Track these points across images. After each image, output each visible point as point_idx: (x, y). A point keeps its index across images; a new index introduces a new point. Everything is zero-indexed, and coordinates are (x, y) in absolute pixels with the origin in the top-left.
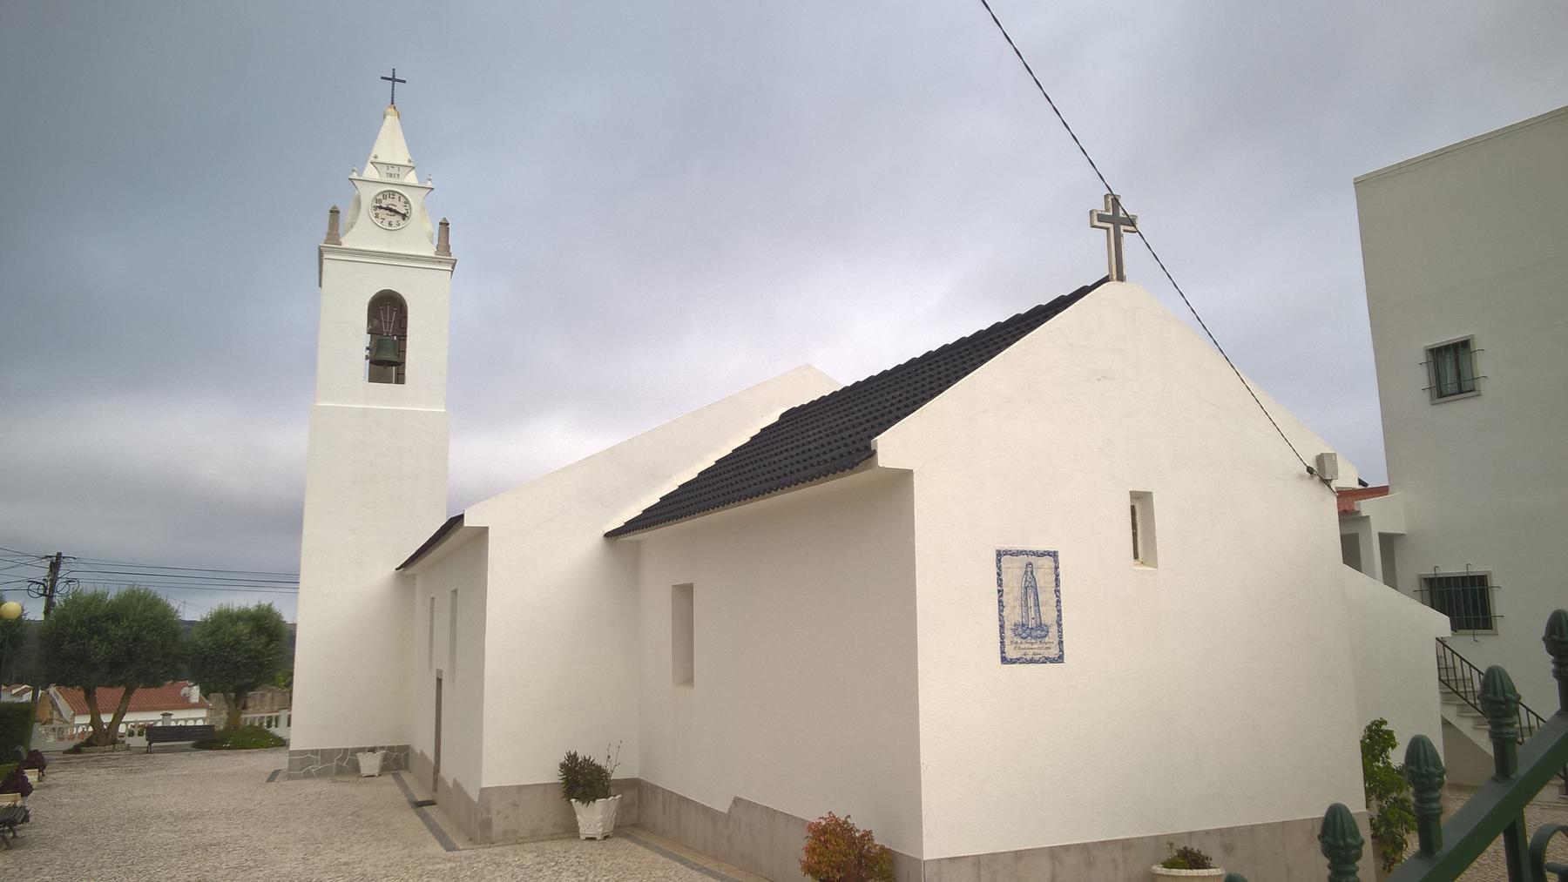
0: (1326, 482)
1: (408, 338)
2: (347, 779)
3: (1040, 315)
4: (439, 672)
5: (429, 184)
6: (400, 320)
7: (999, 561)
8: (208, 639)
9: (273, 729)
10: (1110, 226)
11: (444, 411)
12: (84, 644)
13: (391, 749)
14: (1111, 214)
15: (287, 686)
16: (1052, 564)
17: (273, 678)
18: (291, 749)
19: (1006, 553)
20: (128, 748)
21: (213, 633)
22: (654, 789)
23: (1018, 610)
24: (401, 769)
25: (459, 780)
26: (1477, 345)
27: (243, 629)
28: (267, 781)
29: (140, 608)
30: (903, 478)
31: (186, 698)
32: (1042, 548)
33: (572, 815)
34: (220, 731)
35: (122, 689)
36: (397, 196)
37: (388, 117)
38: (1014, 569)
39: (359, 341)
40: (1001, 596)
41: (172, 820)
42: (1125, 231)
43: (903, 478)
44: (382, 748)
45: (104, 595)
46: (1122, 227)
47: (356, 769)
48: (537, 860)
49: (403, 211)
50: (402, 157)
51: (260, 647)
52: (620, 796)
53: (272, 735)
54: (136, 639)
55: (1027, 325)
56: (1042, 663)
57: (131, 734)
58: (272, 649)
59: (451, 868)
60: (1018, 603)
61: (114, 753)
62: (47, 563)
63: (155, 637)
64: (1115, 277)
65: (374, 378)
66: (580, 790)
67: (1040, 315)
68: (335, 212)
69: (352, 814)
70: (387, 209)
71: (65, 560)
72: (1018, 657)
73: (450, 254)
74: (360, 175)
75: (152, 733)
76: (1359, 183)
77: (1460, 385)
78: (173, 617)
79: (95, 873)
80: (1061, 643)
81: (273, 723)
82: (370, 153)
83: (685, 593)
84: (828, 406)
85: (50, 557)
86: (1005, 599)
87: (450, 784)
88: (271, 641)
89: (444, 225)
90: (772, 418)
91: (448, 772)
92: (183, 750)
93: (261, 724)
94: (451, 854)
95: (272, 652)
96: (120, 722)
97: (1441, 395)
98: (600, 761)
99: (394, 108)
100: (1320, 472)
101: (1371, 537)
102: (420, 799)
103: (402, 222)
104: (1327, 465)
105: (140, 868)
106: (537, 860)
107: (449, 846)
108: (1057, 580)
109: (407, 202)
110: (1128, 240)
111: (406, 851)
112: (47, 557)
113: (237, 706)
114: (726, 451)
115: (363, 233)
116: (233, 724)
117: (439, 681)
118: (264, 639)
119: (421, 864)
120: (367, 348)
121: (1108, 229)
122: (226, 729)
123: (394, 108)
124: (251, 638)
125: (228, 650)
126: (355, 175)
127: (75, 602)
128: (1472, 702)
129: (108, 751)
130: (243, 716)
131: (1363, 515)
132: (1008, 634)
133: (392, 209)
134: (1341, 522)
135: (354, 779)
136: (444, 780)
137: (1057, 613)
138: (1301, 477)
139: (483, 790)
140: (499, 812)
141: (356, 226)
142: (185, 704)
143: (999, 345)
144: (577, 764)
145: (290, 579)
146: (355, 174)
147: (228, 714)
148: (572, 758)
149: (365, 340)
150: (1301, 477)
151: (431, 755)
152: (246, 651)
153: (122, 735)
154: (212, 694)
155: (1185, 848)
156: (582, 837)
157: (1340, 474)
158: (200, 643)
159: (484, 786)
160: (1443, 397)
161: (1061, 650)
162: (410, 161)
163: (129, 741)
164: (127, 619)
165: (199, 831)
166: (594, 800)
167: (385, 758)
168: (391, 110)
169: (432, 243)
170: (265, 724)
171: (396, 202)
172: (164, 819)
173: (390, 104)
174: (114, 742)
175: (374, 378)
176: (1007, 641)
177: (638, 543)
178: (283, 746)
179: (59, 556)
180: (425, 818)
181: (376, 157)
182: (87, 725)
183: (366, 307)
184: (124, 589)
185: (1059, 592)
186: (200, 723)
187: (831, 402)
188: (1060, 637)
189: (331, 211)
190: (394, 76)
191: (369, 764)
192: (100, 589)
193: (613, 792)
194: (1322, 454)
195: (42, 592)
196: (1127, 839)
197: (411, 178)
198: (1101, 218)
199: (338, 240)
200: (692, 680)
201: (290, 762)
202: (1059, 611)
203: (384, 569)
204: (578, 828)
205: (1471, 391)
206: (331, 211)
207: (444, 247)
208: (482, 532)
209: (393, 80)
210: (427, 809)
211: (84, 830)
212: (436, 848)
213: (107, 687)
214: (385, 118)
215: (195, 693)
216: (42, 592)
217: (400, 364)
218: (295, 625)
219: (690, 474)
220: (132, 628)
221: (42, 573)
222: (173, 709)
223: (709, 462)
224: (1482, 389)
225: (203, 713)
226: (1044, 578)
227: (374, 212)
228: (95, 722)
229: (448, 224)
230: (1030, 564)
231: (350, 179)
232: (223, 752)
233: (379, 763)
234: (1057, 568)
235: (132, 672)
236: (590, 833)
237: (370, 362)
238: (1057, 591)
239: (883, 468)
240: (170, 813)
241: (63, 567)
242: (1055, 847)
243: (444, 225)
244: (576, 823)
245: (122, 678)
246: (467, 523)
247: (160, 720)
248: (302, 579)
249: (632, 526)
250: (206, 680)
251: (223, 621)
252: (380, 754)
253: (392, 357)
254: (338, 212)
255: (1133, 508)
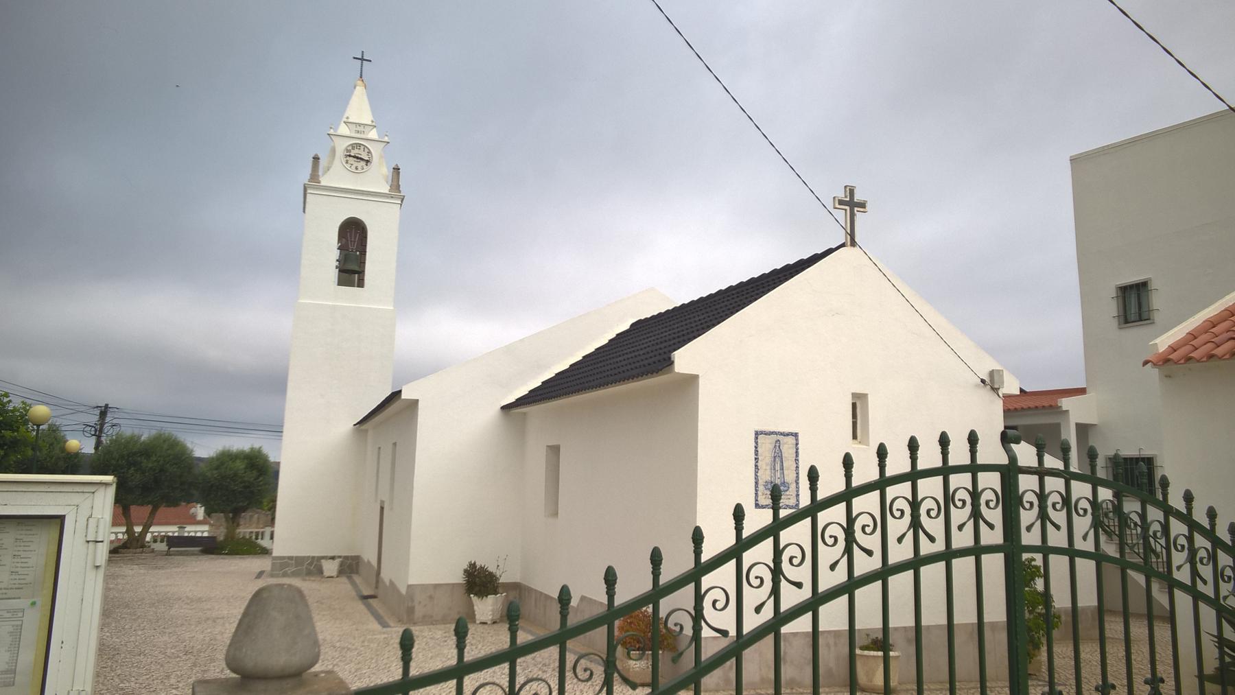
0: (995, 390)
1: (367, 254)
2: (313, 579)
3: (815, 259)
4: (382, 502)
5: (386, 139)
6: (362, 240)
7: (756, 438)
8: (215, 472)
9: (259, 541)
10: (847, 208)
11: (392, 308)
12: (123, 473)
13: (346, 558)
14: (848, 199)
15: (269, 510)
16: (794, 442)
17: (261, 503)
18: (274, 555)
19: (762, 433)
20: (153, 551)
21: (217, 468)
22: (530, 590)
23: (768, 472)
24: (354, 573)
25: (393, 580)
26: (1153, 285)
27: (240, 465)
28: (256, 578)
29: (165, 447)
30: (692, 380)
31: (194, 517)
32: (787, 430)
33: (471, 606)
34: (221, 541)
35: (150, 508)
36: (362, 147)
37: (358, 88)
38: (766, 444)
39: (332, 254)
40: (757, 462)
41: (189, 601)
42: (858, 211)
43: (692, 380)
44: (340, 557)
45: (139, 437)
46: (856, 209)
47: (320, 571)
48: (445, 635)
49: (367, 159)
50: (367, 118)
51: (252, 479)
52: (505, 594)
53: (259, 546)
54: (161, 470)
55: (785, 276)
56: (784, 508)
57: (155, 541)
58: (261, 481)
59: (385, 638)
60: (768, 468)
61: (143, 554)
62: (97, 412)
63: (175, 469)
64: (849, 244)
65: (341, 283)
66: (477, 589)
67: (815, 259)
68: (316, 159)
69: (318, 602)
70: (354, 157)
71: (111, 410)
72: (767, 504)
73: (400, 192)
74: (335, 131)
75: (172, 542)
76: (1073, 160)
77: (1140, 315)
78: (189, 454)
79: (140, 633)
80: (798, 495)
81: (260, 537)
82: (343, 116)
83: (555, 450)
84: (699, 307)
85: (100, 407)
86: (759, 464)
87: (388, 584)
88: (260, 475)
89: (397, 169)
90: (625, 326)
91: (386, 575)
92: (193, 554)
93: (251, 537)
94: (385, 629)
95: (261, 483)
96: (147, 532)
97: (1126, 322)
98: (492, 568)
99: (362, 81)
100: (991, 383)
101: (1069, 426)
102: (366, 593)
103: (365, 167)
104: (996, 378)
105: (170, 631)
106: (445, 635)
107: (384, 625)
108: (797, 452)
109: (369, 152)
110: (859, 217)
111: (354, 626)
112: (98, 407)
113: (233, 523)
114: (590, 349)
115: (337, 175)
116: (230, 536)
117: (382, 508)
118: (255, 473)
119: (364, 635)
120: (337, 261)
121: (846, 210)
122: (225, 540)
123: (362, 81)
124: (245, 472)
125: (228, 480)
126: (332, 132)
127: (116, 442)
128: (1137, 551)
129: (139, 553)
130: (238, 531)
131: (1064, 409)
132: (761, 488)
133: (358, 157)
134: (1005, 417)
135: (319, 579)
136: (383, 582)
137: (795, 475)
138: (977, 386)
139: (409, 586)
140: (420, 602)
141: (331, 170)
142: (193, 521)
143: (781, 279)
144: (475, 571)
145: (277, 430)
146: (332, 130)
147: (227, 528)
148: (473, 565)
149: (335, 254)
150: (977, 386)
151: (374, 563)
152: (241, 483)
153: (148, 542)
154: (213, 514)
155: (877, 638)
156: (478, 622)
157: (1005, 384)
158: (208, 474)
159: (410, 583)
160: (1142, 320)
161: (798, 501)
162: (372, 122)
163: (154, 546)
164: (156, 455)
165: (209, 609)
166: (487, 596)
167: (341, 565)
168: (360, 82)
169: (387, 182)
170: (254, 537)
171: (361, 152)
172: (183, 601)
173: (359, 77)
174: (143, 546)
175: (341, 283)
176: (760, 493)
177: (525, 414)
178: (267, 553)
179: (106, 406)
180: (369, 607)
181: (347, 118)
182: (123, 533)
183: (337, 230)
184: (154, 432)
185: (798, 460)
186: (206, 534)
187: (665, 317)
188: (798, 491)
189: (314, 158)
190: (362, 56)
191: (330, 568)
192: (136, 432)
193: (500, 591)
194: (993, 370)
195: (93, 433)
196: (839, 631)
197: (373, 134)
198: (841, 202)
199: (318, 179)
200: (557, 513)
201: (273, 564)
202: (797, 473)
203: (345, 425)
204: (474, 615)
205: (1147, 320)
206: (314, 158)
207: (396, 186)
208: (415, 403)
209: (362, 59)
210: (371, 601)
211: (127, 606)
212: (376, 626)
213: (139, 505)
214: (355, 88)
215: (200, 511)
216: (93, 433)
217: (361, 273)
218: (279, 463)
219: (564, 365)
220: (159, 462)
221: (94, 419)
222: (186, 524)
223: (578, 357)
224: (1155, 319)
225: (206, 528)
226: (787, 451)
227: (345, 159)
228: (129, 531)
229: (399, 169)
230: (779, 441)
231: (329, 134)
232: (222, 556)
233: (336, 568)
234: (797, 444)
235: (157, 495)
236: (483, 619)
237: (339, 271)
238: (797, 460)
239: (678, 373)
240: (187, 597)
241: (109, 415)
242: (787, 633)
243: (397, 169)
244: (474, 612)
245: (150, 499)
246: (403, 397)
247: (176, 532)
248: (285, 429)
249: (521, 402)
250: (212, 503)
251: (226, 458)
252: (338, 561)
253: (356, 268)
254: (319, 159)
255: (854, 406)
